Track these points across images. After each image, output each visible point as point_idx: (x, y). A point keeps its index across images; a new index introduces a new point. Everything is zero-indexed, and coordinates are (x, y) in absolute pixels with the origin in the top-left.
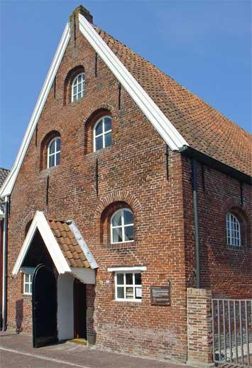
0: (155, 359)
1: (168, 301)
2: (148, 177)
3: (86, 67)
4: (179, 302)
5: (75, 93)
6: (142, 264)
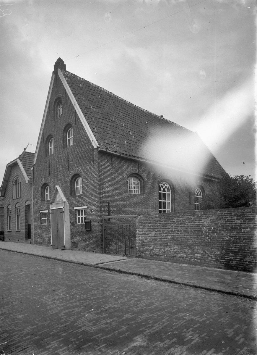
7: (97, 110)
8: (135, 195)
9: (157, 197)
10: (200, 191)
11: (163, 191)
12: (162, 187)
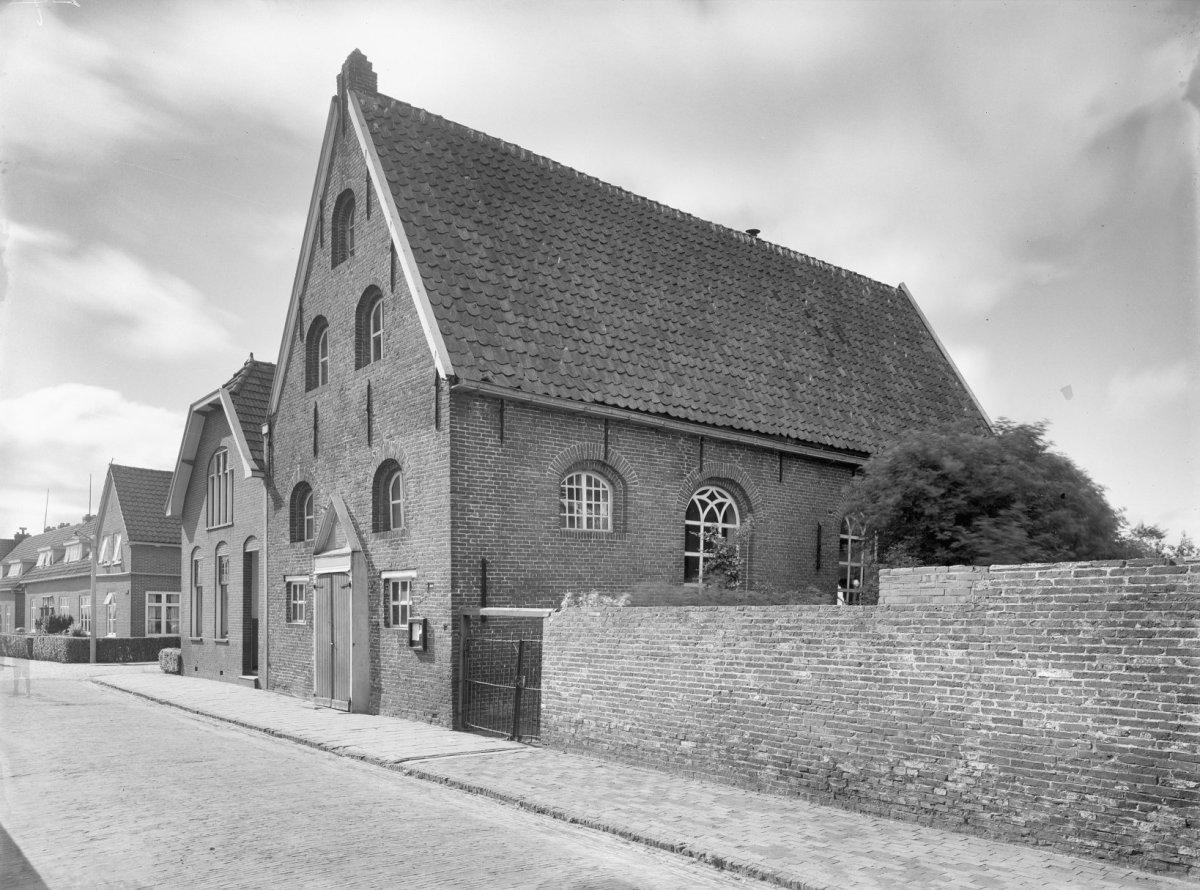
7: (475, 235)
8: (589, 535)
9: (678, 543)
11: (706, 520)
12: (704, 504)
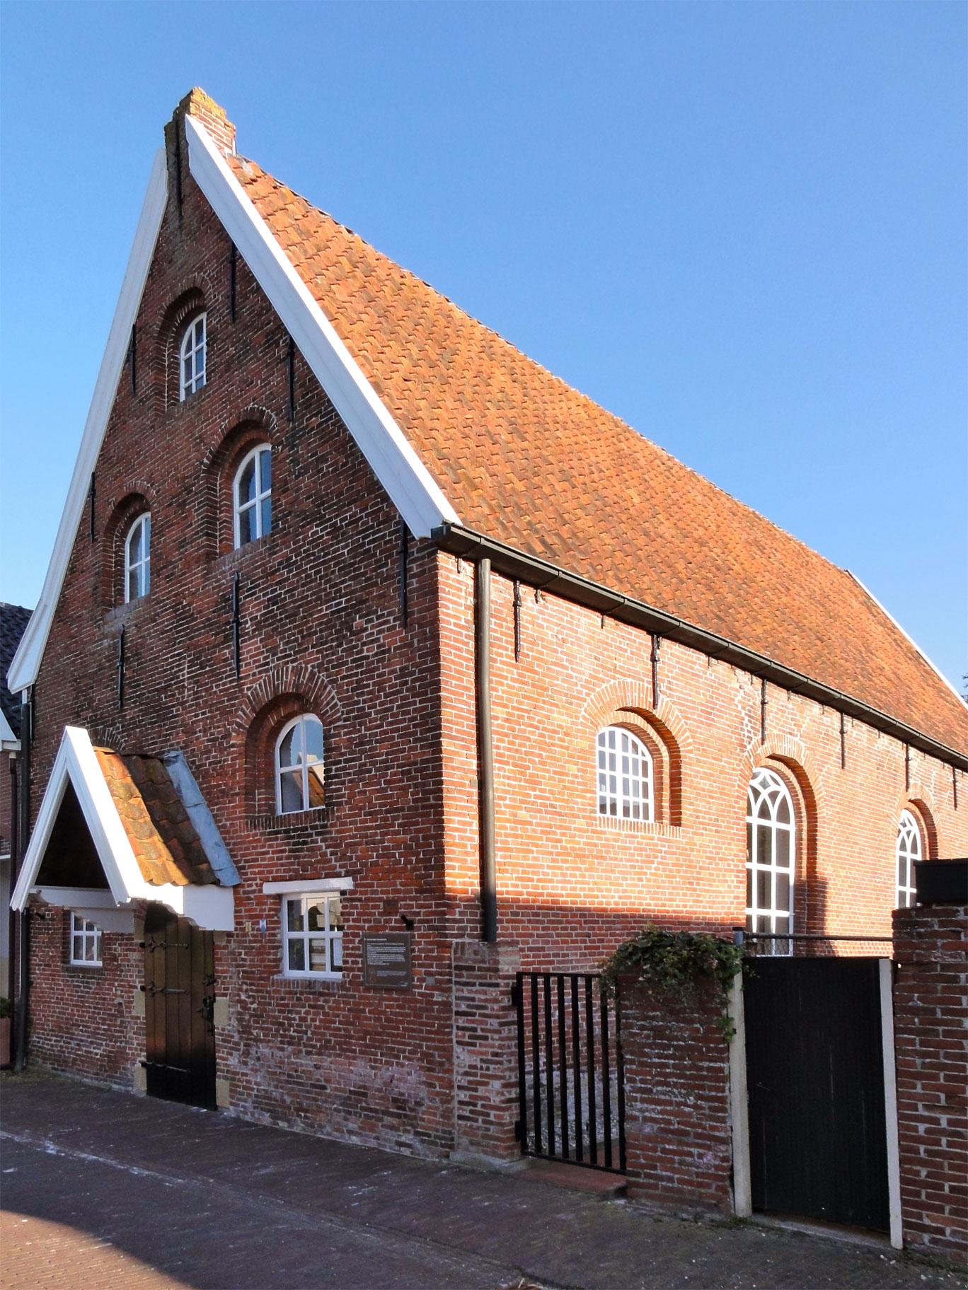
0: (372, 1143)
1: (405, 979)
2: (358, 622)
3: (209, 289)
4: (430, 980)
5: (189, 376)
6: (343, 871)
10: (784, 791)
